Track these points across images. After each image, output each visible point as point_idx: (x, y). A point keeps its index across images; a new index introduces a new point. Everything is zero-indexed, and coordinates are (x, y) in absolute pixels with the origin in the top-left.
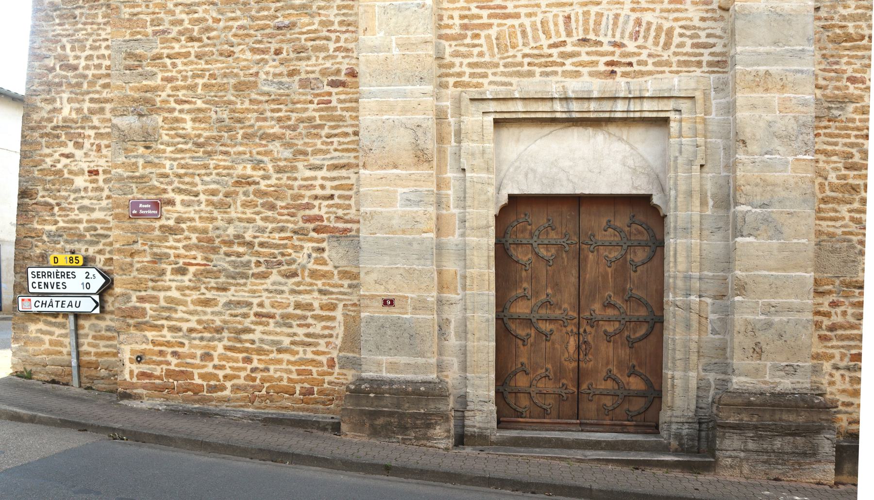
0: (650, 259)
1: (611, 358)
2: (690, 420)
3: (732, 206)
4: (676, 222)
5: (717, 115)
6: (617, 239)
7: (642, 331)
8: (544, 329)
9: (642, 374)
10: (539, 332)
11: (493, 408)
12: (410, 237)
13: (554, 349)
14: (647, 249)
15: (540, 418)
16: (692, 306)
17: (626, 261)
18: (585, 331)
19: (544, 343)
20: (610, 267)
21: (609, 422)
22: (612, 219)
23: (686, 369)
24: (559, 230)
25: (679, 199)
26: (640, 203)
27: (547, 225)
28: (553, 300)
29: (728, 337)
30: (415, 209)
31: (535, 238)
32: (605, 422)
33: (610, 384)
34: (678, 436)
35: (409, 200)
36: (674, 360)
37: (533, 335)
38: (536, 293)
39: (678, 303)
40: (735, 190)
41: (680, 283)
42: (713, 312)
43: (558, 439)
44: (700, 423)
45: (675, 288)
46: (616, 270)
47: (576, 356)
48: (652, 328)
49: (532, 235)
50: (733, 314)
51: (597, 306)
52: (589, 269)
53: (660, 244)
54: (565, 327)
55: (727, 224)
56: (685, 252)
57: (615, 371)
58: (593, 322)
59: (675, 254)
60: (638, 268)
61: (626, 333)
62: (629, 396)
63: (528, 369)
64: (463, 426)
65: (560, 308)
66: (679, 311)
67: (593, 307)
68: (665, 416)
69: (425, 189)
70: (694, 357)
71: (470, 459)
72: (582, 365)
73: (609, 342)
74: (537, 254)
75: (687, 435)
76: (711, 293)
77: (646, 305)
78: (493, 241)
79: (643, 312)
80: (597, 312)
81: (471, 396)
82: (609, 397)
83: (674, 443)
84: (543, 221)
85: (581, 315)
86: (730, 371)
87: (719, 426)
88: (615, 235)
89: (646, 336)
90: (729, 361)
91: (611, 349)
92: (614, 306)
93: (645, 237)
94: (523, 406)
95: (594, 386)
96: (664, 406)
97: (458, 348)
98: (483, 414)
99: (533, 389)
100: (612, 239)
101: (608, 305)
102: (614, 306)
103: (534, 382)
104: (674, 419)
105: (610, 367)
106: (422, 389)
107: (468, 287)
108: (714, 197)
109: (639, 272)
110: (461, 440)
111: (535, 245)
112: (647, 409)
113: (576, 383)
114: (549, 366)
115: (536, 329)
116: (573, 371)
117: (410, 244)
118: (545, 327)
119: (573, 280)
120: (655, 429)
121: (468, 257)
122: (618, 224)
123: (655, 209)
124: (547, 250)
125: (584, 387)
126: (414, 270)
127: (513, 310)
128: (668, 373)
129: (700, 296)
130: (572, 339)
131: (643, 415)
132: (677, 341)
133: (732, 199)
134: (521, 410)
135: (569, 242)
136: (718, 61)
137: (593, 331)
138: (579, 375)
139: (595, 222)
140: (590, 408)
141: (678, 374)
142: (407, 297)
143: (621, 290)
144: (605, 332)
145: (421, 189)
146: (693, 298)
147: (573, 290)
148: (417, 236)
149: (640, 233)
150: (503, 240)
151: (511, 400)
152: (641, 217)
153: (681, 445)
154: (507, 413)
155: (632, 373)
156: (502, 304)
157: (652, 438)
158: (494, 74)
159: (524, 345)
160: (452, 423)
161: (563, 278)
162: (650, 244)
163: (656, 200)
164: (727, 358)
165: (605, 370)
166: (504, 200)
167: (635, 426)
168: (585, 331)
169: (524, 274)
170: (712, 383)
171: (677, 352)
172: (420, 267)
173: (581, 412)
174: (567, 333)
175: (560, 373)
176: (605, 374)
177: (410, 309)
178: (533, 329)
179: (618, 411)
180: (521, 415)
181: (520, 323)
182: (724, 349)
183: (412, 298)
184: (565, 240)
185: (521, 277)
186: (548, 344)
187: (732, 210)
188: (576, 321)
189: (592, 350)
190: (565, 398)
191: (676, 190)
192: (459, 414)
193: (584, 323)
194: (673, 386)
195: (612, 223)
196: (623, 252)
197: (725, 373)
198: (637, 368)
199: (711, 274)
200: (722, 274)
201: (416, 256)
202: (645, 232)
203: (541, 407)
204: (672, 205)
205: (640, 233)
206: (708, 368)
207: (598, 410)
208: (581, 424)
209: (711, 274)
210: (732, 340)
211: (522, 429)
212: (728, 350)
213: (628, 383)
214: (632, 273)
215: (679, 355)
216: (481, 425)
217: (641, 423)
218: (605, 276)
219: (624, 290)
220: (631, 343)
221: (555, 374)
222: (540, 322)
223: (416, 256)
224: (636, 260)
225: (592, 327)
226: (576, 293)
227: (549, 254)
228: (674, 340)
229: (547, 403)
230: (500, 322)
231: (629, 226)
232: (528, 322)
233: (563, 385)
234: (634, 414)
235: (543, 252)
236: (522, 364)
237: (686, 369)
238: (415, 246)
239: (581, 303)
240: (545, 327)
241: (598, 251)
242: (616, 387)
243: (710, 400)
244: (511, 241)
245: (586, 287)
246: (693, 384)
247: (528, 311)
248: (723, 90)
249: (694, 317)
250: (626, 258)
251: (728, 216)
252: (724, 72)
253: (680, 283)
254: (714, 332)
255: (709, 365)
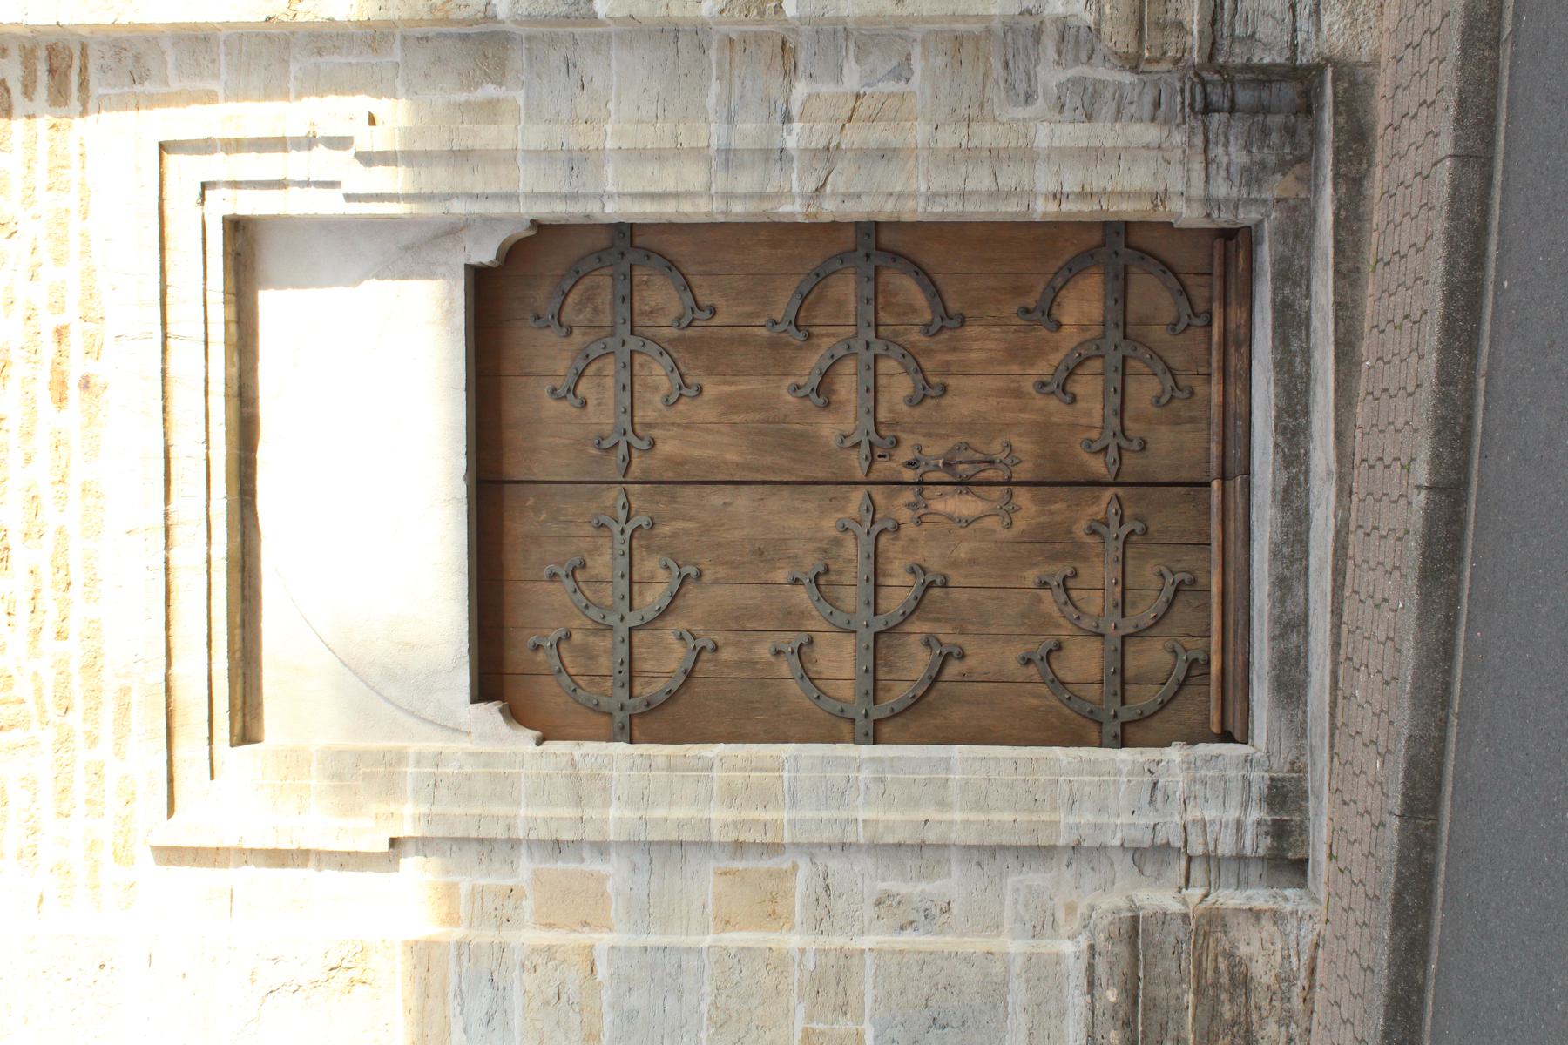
0: (671, 265)
1: (999, 383)
2: (1199, 140)
3: (498, 27)
4: (550, 196)
5: (216, 76)
6: (610, 365)
7: (907, 287)
8: (908, 594)
9: (1049, 284)
10: (918, 607)
11: (1175, 753)
12: (608, 1018)
13: (973, 561)
14: (640, 275)
15: (1207, 605)
16: (818, 142)
17: (679, 340)
18: (912, 464)
19: (955, 594)
20: (700, 390)
21: (1216, 388)
22: (547, 385)
23: (1027, 156)
24: (583, 544)
25: (479, 189)
26: (492, 304)
27: (570, 584)
28: (811, 564)
29: (918, 31)
30: (517, 1001)
31: (612, 619)
32: (1216, 399)
33: (1088, 387)
34: (1253, 176)
35: (490, 1017)
36: (995, 195)
37: (927, 627)
38: (790, 618)
39: (811, 186)
40: (446, 21)
41: (746, 182)
42: (839, 75)
43: (1274, 556)
44: (1208, 109)
45: (762, 196)
46: (710, 370)
47: (996, 492)
48: (896, 255)
49: (604, 629)
50: (839, 19)
51: (829, 429)
52: (706, 453)
53: (625, 235)
54: (897, 527)
55: (553, 41)
56: (644, 157)
57: (1043, 368)
58: (881, 443)
59: (652, 196)
60: (704, 300)
61: (915, 336)
62: (1121, 319)
63: (1038, 646)
64: (1240, 858)
65: (837, 542)
66: (838, 182)
67: (834, 443)
68: (1187, 214)
69: (452, 968)
70: (987, 134)
71: (1353, 823)
72: (1022, 473)
73: (944, 389)
74: (663, 613)
75: (1247, 148)
76: (776, 82)
77: (820, 277)
78: (621, 748)
79: (846, 289)
80: (848, 426)
81: (1136, 834)
82: (1132, 386)
83: (1278, 186)
84: (560, 593)
85: (860, 476)
86: (1029, 22)
87: (1211, 57)
88: (599, 374)
89: (920, 272)
90: (996, 25)
91: (965, 382)
92: (826, 380)
93: (603, 283)
94: (1169, 658)
95: (1094, 434)
96: (1159, 216)
97: (975, 872)
98: (1197, 788)
99: (1108, 629)
100: (610, 382)
101: (823, 390)
102: (826, 380)
103: (1086, 623)
104: (1197, 189)
105: (1028, 385)
106: (1112, 996)
107: (770, 838)
108: (470, 83)
109: (717, 300)
110: (1285, 859)
111: (633, 620)
112: (1168, 267)
113: (1087, 492)
114: (1031, 576)
115: (907, 617)
116: (1042, 502)
117: (631, 1017)
118: (899, 592)
119: (743, 500)
120: (1232, 243)
121: (674, 837)
122: (562, 366)
123: (513, 252)
124: (651, 581)
125: (1098, 466)
126: (715, 1005)
127: (847, 691)
128: (1043, 209)
129: (787, 118)
130: (938, 505)
131: (1190, 281)
132: (935, 187)
133: (476, 29)
134: (1181, 669)
135: (622, 515)
136: (51, 71)
137: (909, 440)
138: (1057, 481)
139: (553, 429)
140: (1172, 447)
141: (1045, 181)
142: (805, 1030)
143: (777, 353)
144: (914, 402)
145: (454, 980)
146: (791, 143)
147: (780, 501)
148: (607, 996)
149: (588, 299)
150: (620, 717)
151: (1144, 697)
152: (542, 296)
153: (1283, 166)
154: (1193, 699)
155: (1046, 314)
156: (831, 725)
157: (1266, 255)
158: (93, 740)
159: (962, 656)
160: (1229, 898)
161: (736, 535)
162: (624, 267)
163: (486, 254)
164: (989, 30)
165: (1040, 401)
166: (490, 712)
167: (1225, 305)
168: (912, 464)
169: (727, 654)
170: (1072, 72)
171: (970, 186)
172: (707, 988)
173: (1185, 475)
174: (919, 521)
175: (1050, 541)
176: (1054, 404)
177: (844, 1026)
178: (907, 628)
179: (1176, 360)
180: (1197, 667)
181: (891, 666)
182: (958, 40)
183: (810, 1018)
184: (616, 528)
185: (739, 664)
186: (956, 578)
187: (509, 27)
188: (877, 492)
189: (975, 441)
190: (1138, 527)
191: (448, 197)
192: (1198, 873)
193: (883, 468)
194: (1083, 195)
195: (559, 382)
196: (652, 348)
197: (1037, 35)
198: (1030, 301)
199: (715, 87)
200: (713, 54)
201: (671, 1003)
202: (587, 281)
203: (1170, 604)
204: (497, 208)
205: (588, 299)
206: (1022, 87)
207: (1176, 421)
208: (1224, 477)
209: (715, 87)
210: (925, 20)
211: (1247, 665)
212: (960, 27)
213: (1081, 327)
214: (716, 321)
215: (981, 180)
216: (1235, 798)
217: (1217, 285)
218: (730, 405)
219: (775, 345)
220: (948, 320)
221: (1055, 557)
222: (883, 604)
223: (671, 1003)
224: (675, 308)
225: (896, 443)
226: (786, 492)
227: (662, 575)
228: (932, 196)
229: (1155, 583)
230: (886, 730)
231: (570, 332)
232: (882, 643)
233: (1094, 532)
234: (1170, 383)
235: (653, 597)
236: (1027, 661)
237: (1027, 156)
238: (636, 1001)
239: (820, 475)
240: (897, 597)
241: (649, 426)
242: (1096, 365)
243: (1127, 78)
244: (623, 694)
245: (769, 460)
246: (1074, 133)
247: (849, 643)
248: (137, 58)
249: (854, 137)
250: (670, 341)
251: (530, 38)
252: (84, 54)
253: (746, 182)
254: (902, 72)
255: (1010, 86)
